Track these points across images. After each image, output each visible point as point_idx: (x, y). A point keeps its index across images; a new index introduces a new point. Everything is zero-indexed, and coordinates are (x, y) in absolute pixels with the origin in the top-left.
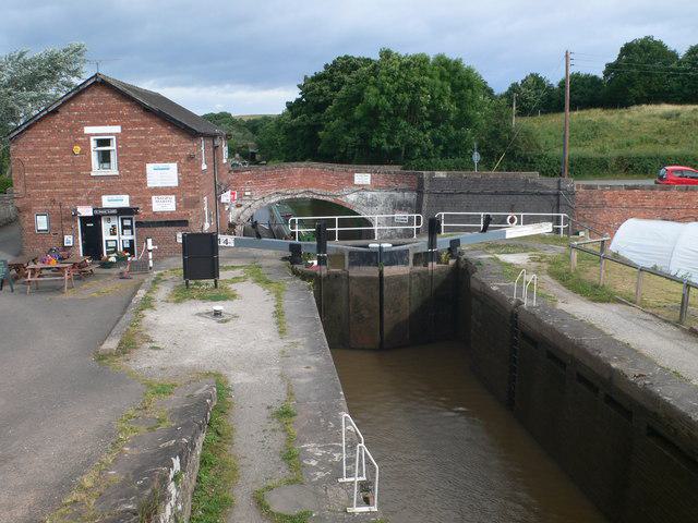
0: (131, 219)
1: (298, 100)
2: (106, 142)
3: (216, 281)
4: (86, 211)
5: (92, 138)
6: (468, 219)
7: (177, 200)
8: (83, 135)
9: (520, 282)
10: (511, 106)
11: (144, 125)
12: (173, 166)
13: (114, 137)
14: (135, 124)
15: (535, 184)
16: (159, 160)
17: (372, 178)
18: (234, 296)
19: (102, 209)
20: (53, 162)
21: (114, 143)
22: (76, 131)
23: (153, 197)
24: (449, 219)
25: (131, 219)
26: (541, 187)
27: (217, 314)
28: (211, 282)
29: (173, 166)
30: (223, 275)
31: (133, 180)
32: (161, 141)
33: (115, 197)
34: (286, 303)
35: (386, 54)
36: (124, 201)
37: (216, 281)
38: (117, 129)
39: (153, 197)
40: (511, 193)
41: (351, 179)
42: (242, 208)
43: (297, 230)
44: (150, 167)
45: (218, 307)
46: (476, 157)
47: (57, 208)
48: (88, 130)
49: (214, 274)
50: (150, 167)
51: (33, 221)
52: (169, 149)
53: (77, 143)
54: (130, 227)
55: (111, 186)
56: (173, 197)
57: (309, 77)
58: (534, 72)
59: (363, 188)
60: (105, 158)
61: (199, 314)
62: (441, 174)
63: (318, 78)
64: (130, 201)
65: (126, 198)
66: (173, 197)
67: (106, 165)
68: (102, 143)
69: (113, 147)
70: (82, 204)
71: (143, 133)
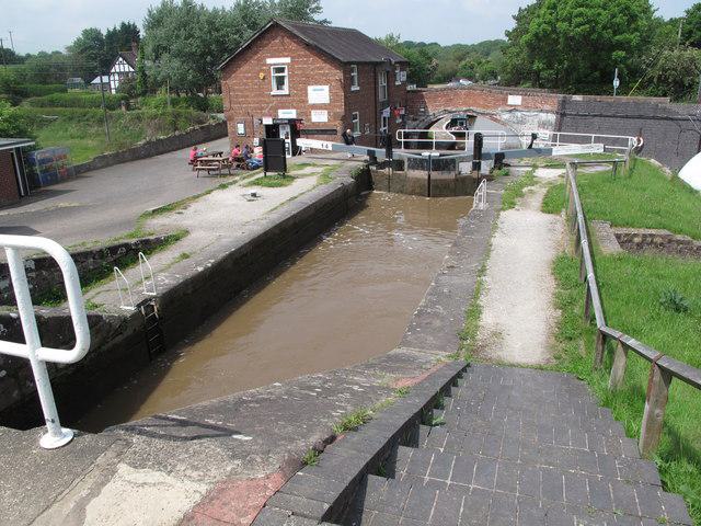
2: (282, 70)
4: (268, 121)
8: (265, 65)
12: (326, 88)
15: (665, 109)
16: (317, 83)
17: (523, 100)
18: (187, 232)
20: (246, 84)
26: (669, 111)
31: (298, 99)
35: (688, 12)
36: (292, 114)
38: (288, 60)
40: (640, 117)
41: (505, 100)
46: (616, 83)
48: (269, 61)
51: (235, 128)
52: (323, 75)
55: (284, 102)
59: (514, 109)
60: (280, 82)
61: (150, 246)
62: (578, 98)
65: (294, 111)
69: (286, 74)
70: (266, 115)
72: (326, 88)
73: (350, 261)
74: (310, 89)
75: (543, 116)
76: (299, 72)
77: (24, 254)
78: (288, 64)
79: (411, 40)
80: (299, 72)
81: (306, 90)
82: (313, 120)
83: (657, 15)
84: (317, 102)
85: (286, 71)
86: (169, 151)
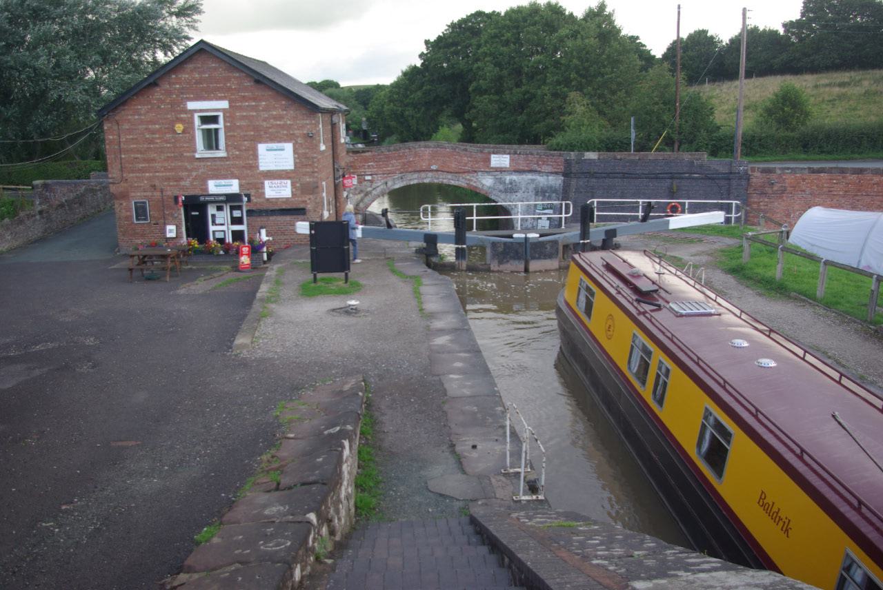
2: (214, 119)
17: (512, 160)
20: (151, 141)
31: (245, 165)
36: (233, 186)
38: (225, 104)
48: (191, 105)
52: (282, 127)
60: (211, 139)
65: (235, 183)
69: (221, 125)
72: (289, 147)
73: (565, 561)
74: (262, 148)
75: (542, 180)
76: (243, 123)
77: (305, 217)
78: (224, 110)
79: (483, 10)
80: (243, 123)
81: (255, 150)
82: (267, 196)
83: (623, 33)
84: (272, 167)
85: (221, 120)
86: (258, 61)
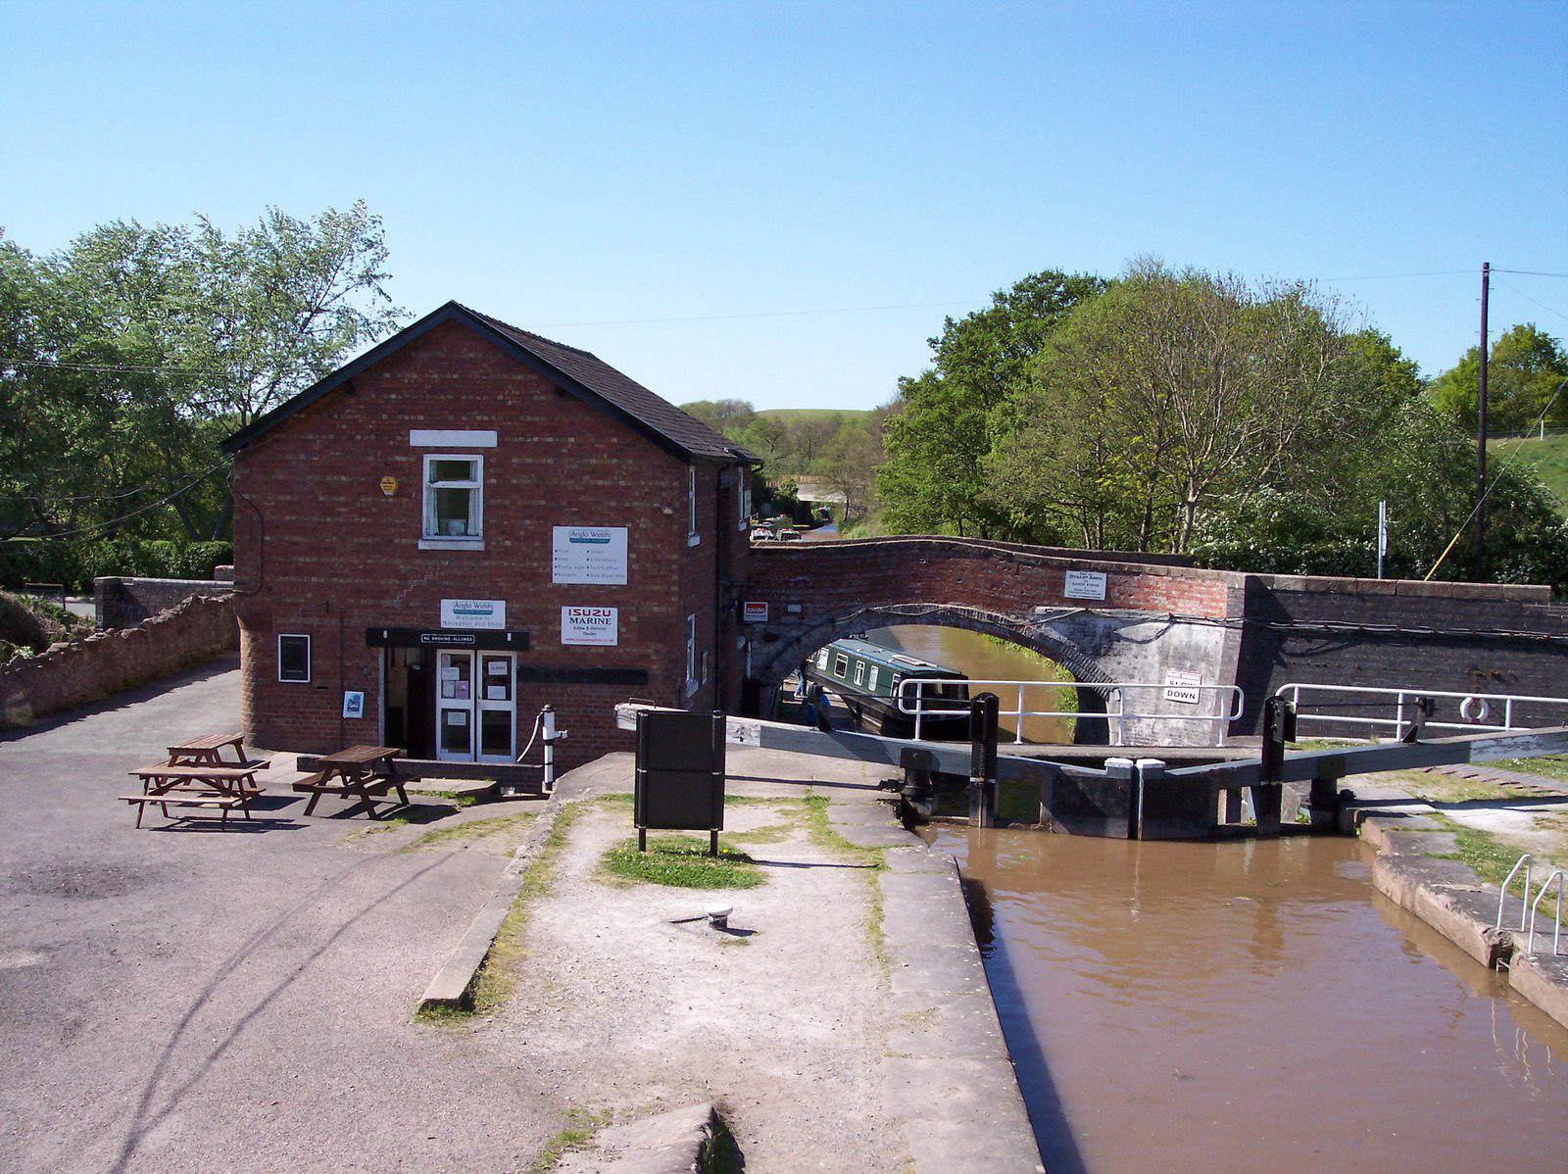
0: (508, 660)
1: (929, 377)
2: (462, 470)
3: (714, 836)
5: (428, 458)
6: (1355, 703)
7: (622, 619)
9: (1517, 886)
10: (336, 584)
11: (553, 431)
12: (619, 536)
13: (480, 459)
14: (532, 429)
19: (1104, 570)
21: (479, 471)
22: (391, 440)
23: (565, 610)
24: (1311, 701)
25: (508, 660)
27: (720, 923)
28: (705, 835)
29: (619, 536)
30: (735, 819)
32: (594, 472)
33: (472, 604)
34: (889, 906)
36: (494, 615)
37: (714, 836)
38: (488, 439)
39: (565, 610)
42: (779, 644)
43: (1399, 722)
44: (561, 535)
45: (716, 901)
47: (333, 622)
48: (418, 438)
49: (713, 820)
50: (561, 535)
53: (393, 469)
54: (503, 681)
55: (467, 577)
56: (614, 611)
57: (956, 321)
58: (1523, 322)
60: (454, 506)
63: (980, 321)
64: (509, 614)
66: (614, 611)
67: (457, 524)
68: (447, 470)
71: (549, 450)
